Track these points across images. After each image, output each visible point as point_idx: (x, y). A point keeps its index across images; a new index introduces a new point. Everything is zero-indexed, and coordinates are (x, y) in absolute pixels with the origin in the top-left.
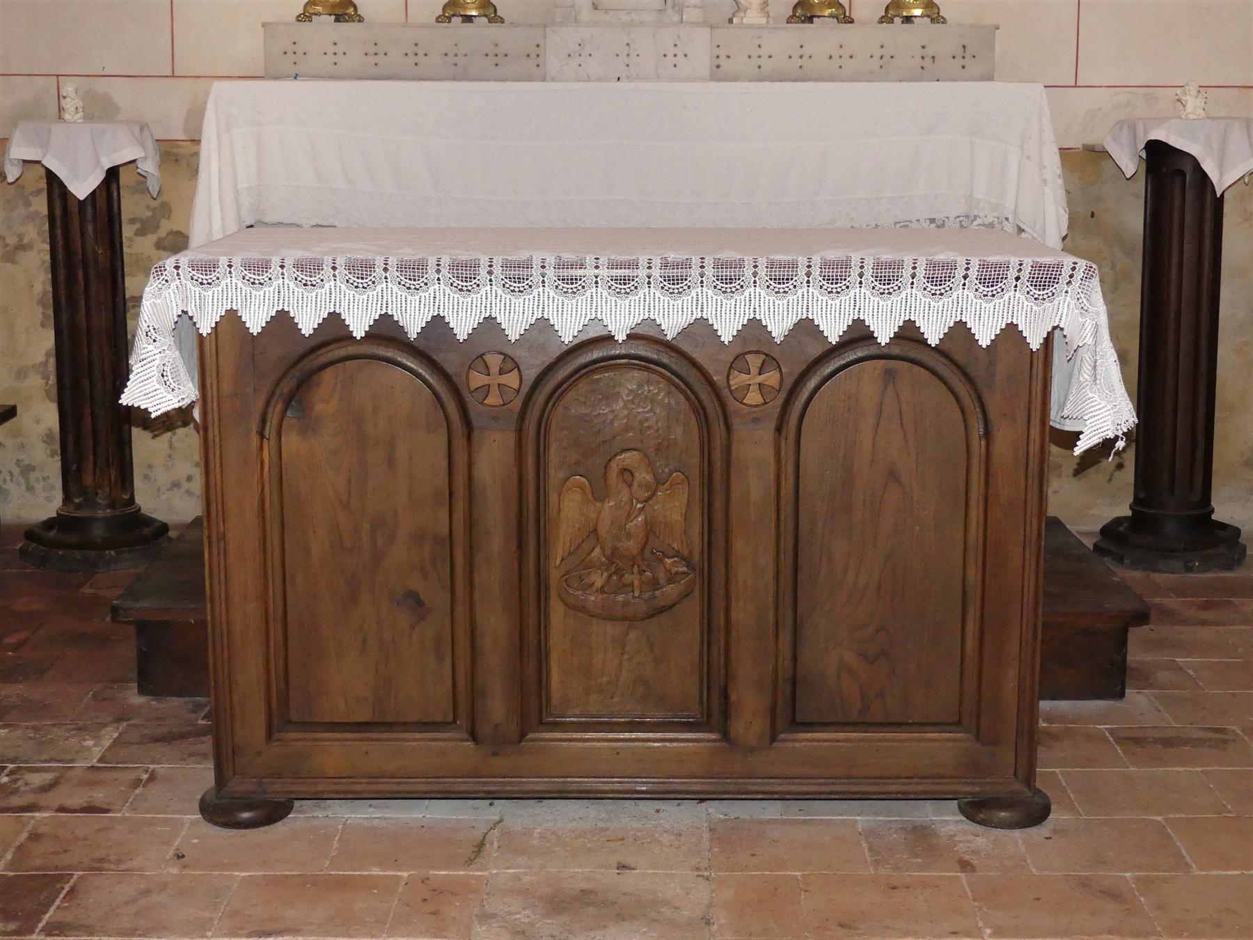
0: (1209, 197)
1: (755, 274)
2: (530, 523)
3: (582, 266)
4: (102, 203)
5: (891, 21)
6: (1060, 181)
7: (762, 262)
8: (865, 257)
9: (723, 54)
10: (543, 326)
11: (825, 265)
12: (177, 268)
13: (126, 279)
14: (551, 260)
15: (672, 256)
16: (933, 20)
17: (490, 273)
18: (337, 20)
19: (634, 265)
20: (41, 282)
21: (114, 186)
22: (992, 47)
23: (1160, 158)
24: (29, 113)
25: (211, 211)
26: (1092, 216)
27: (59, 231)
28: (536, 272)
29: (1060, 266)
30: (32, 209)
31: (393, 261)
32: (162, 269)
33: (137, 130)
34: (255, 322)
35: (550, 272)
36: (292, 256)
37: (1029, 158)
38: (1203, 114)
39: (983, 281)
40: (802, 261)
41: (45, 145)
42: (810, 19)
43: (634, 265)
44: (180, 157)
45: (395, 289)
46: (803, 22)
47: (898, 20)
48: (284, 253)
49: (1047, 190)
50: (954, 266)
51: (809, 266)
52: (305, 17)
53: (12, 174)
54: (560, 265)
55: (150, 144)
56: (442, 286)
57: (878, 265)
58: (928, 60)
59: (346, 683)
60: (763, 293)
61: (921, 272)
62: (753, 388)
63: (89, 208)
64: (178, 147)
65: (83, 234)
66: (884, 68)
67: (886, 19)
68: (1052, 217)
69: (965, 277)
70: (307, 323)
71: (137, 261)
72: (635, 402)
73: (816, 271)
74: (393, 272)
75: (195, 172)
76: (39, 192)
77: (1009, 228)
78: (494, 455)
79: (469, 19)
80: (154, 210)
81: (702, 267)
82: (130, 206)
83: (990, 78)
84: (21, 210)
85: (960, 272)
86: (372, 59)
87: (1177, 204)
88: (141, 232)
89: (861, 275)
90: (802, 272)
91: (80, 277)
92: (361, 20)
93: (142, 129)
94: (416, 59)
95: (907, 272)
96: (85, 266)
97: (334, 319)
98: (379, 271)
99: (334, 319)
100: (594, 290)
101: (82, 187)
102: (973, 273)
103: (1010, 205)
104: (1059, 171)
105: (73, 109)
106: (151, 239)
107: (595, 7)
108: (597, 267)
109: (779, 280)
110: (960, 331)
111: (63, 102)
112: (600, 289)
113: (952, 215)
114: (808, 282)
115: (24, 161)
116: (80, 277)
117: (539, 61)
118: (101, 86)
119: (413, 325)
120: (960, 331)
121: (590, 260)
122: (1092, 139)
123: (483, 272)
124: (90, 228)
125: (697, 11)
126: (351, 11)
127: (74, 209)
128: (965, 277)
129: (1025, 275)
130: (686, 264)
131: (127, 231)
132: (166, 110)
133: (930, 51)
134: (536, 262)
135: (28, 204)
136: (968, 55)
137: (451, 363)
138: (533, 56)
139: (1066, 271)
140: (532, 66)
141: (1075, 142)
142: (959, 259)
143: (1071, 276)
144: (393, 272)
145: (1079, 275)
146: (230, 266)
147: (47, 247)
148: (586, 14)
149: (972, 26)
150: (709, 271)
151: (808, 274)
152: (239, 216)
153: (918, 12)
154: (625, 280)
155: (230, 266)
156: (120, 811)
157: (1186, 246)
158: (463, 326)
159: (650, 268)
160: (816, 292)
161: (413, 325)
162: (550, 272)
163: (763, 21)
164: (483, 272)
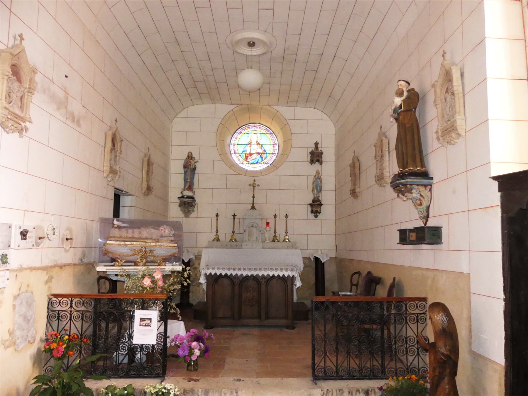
2: (240, 296)
8: (289, 268)
10: (242, 275)
23: (317, 259)
34: (213, 274)
52: (213, 241)
59: (220, 315)
62: (263, 281)
66: (283, 248)
70: (218, 274)
72: (252, 283)
78: (237, 287)
97: (221, 274)
99: (221, 274)
110: (284, 275)
119: (229, 274)
120: (284, 275)
132: (196, 251)
137: (232, 278)
140: (240, 247)
156: (166, 277)
158: (234, 274)
161: (229, 274)
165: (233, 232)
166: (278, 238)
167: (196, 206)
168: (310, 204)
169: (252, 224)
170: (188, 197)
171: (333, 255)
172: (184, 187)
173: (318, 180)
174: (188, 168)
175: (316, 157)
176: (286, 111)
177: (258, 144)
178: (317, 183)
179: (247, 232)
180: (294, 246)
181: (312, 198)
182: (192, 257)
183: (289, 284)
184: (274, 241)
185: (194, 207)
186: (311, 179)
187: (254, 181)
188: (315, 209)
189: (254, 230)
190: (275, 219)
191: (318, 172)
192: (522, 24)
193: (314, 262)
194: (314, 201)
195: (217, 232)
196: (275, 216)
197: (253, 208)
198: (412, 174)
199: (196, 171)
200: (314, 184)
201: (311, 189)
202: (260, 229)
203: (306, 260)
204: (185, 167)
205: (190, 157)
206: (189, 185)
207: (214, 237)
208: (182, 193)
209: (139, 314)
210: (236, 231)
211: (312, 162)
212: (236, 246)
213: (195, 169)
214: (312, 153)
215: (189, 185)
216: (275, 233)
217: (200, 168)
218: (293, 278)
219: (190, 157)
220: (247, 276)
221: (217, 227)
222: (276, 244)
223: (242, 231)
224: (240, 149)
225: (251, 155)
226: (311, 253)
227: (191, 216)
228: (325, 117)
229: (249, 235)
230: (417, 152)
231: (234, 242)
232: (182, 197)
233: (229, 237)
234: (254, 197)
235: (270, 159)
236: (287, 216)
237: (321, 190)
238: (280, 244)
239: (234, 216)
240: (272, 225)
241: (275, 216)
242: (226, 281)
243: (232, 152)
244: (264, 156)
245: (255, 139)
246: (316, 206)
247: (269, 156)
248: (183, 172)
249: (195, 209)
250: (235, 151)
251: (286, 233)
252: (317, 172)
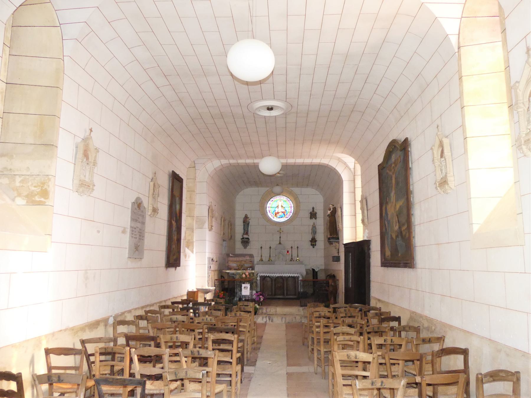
23: (313, 270)
78: (273, 282)
140: (274, 264)
170: (246, 238)
171: (323, 268)
175: (313, 215)
176: (296, 190)
177: (282, 207)
178: (314, 231)
180: (301, 263)
183: (297, 280)
191: (314, 224)
194: (312, 239)
197: (280, 243)
198: (333, 238)
203: (307, 271)
204: (244, 222)
205: (246, 217)
206: (246, 232)
209: (243, 285)
211: (311, 218)
214: (311, 213)
215: (246, 232)
217: (252, 222)
218: (298, 277)
219: (246, 217)
220: (278, 277)
222: (292, 262)
224: (272, 210)
225: (278, 213)
226: (309, 267)
228: (319, 193)
231: (270, 261)
232: (243, 238)
235: (289, 215)
239: (270, 248)
240: (290, 252)
242: (268, 279)
243: (268, 212)
244: (286, 213)
245: (280, 204)
246: (313, 242)
251: (298, 256)
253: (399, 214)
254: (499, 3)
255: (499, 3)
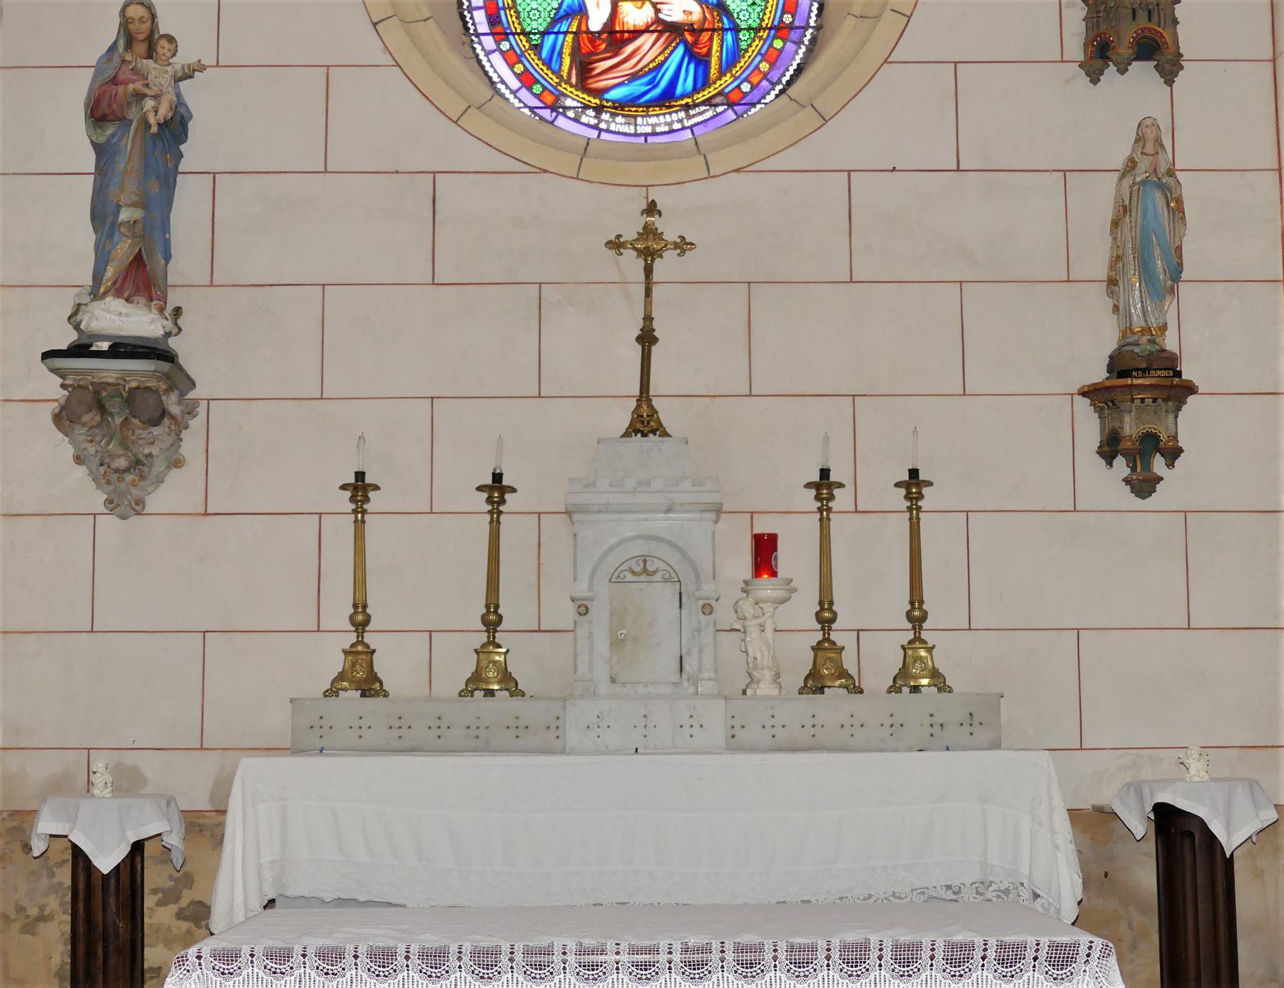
0: (1219, 857)
1: (775, 959)
3: (603, 952)
4: (125, 874)
5: (899, 691)
6: (1072, 847)
7: (782, 946)
9: (737, 723)
11: (845, 948)
12: (199, 957)
13: (146, 950)
14: (572, 946)
15: (693, 941)
16: (939, 690)
17: (511, 960)
18: (363, 695)
19: (654, 950)
20: (60, 954)
21: (138, 859)
22: (998, 714)
23: (1171, 823)
24: (59, 787)
25: (233, 888)
26: (1106, 875)
27: (81, 905)
28: (557, 958)
29: (1076, 945)
30: (55, 880)
31: (414, 949)
32: (183, 959)
33: (163, 804)
35: (571, 958)
36: (313, 944)
37: (1040, 825)
38: (1207, 777)
39: (1001, 961)
40: (822, 944)
41: (73, 819)
42: (821, 690)
43: (654, 950)
44: (206, 828)
45: (416, 977)
46: (814, 693)
47: (906, 690)
48: (306, 941)
49: (1059, 855)
50: (972, 947)
51: (829, 950)
52: (332, 692)
53: (38, 847)
54: (581, 951)
55: (175, 816)
56: (463, 974)
57: (896, 947)
58: (937, 728)
60: (783, 977)
61: (939, 954)
63: (113, 881)
64: (204, 817)
65: (104, 908)
66: (893, 737)
67: (894, 689)
68: (1067, 886)
69: (984, 958)
71: (157, 931)
73: (835, 955)
74: (414, 960)
75: (219, 842)
76: (64, 862)
77: (1025, 894)
79: (490, 693)
80: (176, 880)
81: (723, 952)
82: (154, 877)
83: (996, 745)
84: (45, 882)
85: (978, 954)
86: (397, 732)
87: (1188, 861)
88: (160, 903)
89: (880, 958)
90: (822, 955)
91: (100, 951)
92: (386, 695)
93: (168, 803)
94: (439, 732)
95: (926, 954)
96: (105, 940)
98: (401, 960)
100: (615, 976)
101: (105, 862)
102: (991, 954)
103: (1024, 869)
104: (1070, 837)
105: (102, 784)
106: (173, 908)
107: (613, 680)
108: (618, 953)
109: (799, 964)
111: (93, 778)
112: (621, 976)
113: (968, 882)
114: (828, 965)
115: (51, 836)
116: (100, 951)
117: (560, 732)
118: (130, 758)
121: (610, 945)
122: (1101, 801)
123: (504, 959)
124: (112, 901)
125: (712, 683)
126: (377, 686)
127: (98, 883)
128: (984, 958)
129: (1043, 955)
130: (707, 949)
131: (149, 901)
133: (938, 719)
134: (557, 949)
135: (52, 875)
136: (976, 723)
138: (553, 728)
139: (1083, 950)
140: (551, 740)
141: (1085, 802)
142: (976, 940)
143: (1088, 955)
144: (414, 960)
145: (1096, 954)
146: (252, 956)
147: (69, 918)
148: (604, 687)
149: (978, 695)
150: (730, 956)
151: (828, 958)
152: (261, 890)
153: (925, 682)
154: (645, 966)
155: (252, 956)
157: (1200, 906)
159: (670, 953)
160: (836, 976)
162: (571, 958)
163: (776, 692)
164: (504, 959)
165: (492, 621)
166: (849, 663)
167: (196, 424)
168: (1090, 392)
169: (638, 549)
170: (123, 349)
172: (97, 277)
173: (1150, 196)
174: (123, 120)
179: (600, 613)
181: (1110, 343)
182: (150, 823)
184: (814, 684)
185: (180, 426)
186: (1100, 198)
187: (652, 209)
188: (1130, 427)
189: (660, 599)
190: (824, 511)
191: (1148, 139)
192: (1274, 130)
193: (1150, 846)
194: (1120, 366)
195: (361, 622)
196: (824, 484)
197: (645, 423)
199: (193, 153)
200: (1126, 231)
201: (1098, 267)
202: (708, 589)
204: (102, 112)
207: (337, 663)
208: (74, 320)
210: (513, 610)
212: (518, 728)
213: (176, 128)
216: (826, 618)
221: (360, 582)
223: (560, 613)
227: (155, 502)
229: (617, 644)
230: (81, 965)
232: (80, 350)
233: (458, 662)
234: (647, 338)
236: (914, 483)
237: (1176, 273)
238: (874, 706)
240: (796, 558)
241: (824, 484)
247: (752, 47)
248: (88, 160)
249: (191, 444)
250: (493, 20)
252: (1140, 140)
253: (159, 474)
254: (648, 318)
255: (648, 318)
